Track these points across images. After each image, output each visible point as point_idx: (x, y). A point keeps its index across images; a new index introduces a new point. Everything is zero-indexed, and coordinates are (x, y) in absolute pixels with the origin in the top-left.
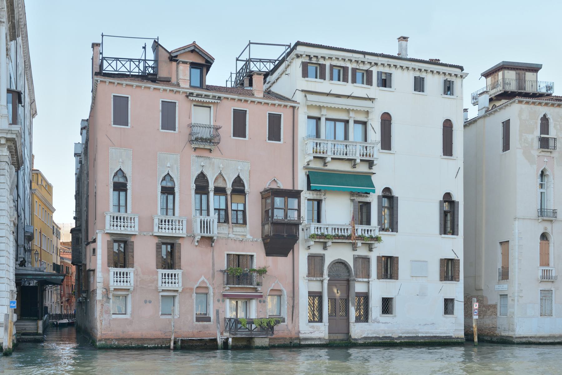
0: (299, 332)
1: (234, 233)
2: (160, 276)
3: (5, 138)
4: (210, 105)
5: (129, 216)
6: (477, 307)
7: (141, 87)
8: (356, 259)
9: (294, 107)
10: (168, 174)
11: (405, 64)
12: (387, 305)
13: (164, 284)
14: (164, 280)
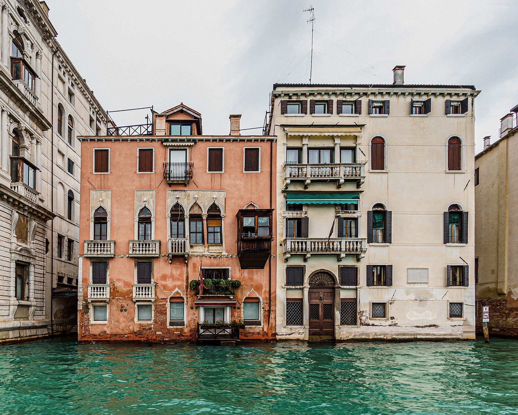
0: (276, 334)
1: (210, 251)
4: (186, 148)
6: (487, 310)
8: (343, 270)
11: (399, 90)
12: (380, 309)
14: (138, 293)
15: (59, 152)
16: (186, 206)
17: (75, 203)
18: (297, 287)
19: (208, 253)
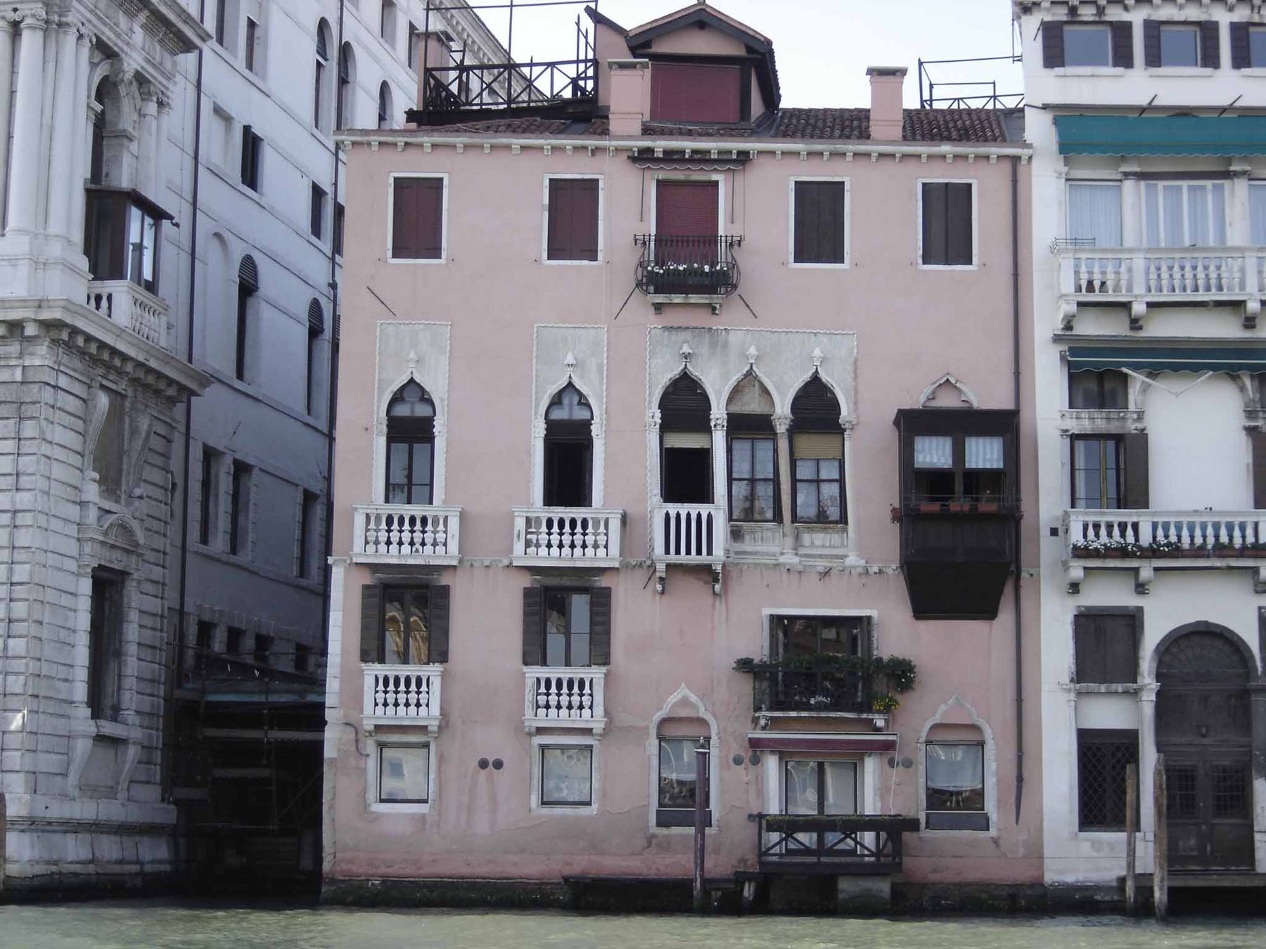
2: (369, 681)
3: (35, 321)
5: (602, 516)
7: (481, 147)
9: (1015, 160)
10: (570, 385)
13: (542, 711)
15: (218, 111)
16: (718, 388)
17: (263, 304)
18: (1114, 687)
19: (796, 560)
